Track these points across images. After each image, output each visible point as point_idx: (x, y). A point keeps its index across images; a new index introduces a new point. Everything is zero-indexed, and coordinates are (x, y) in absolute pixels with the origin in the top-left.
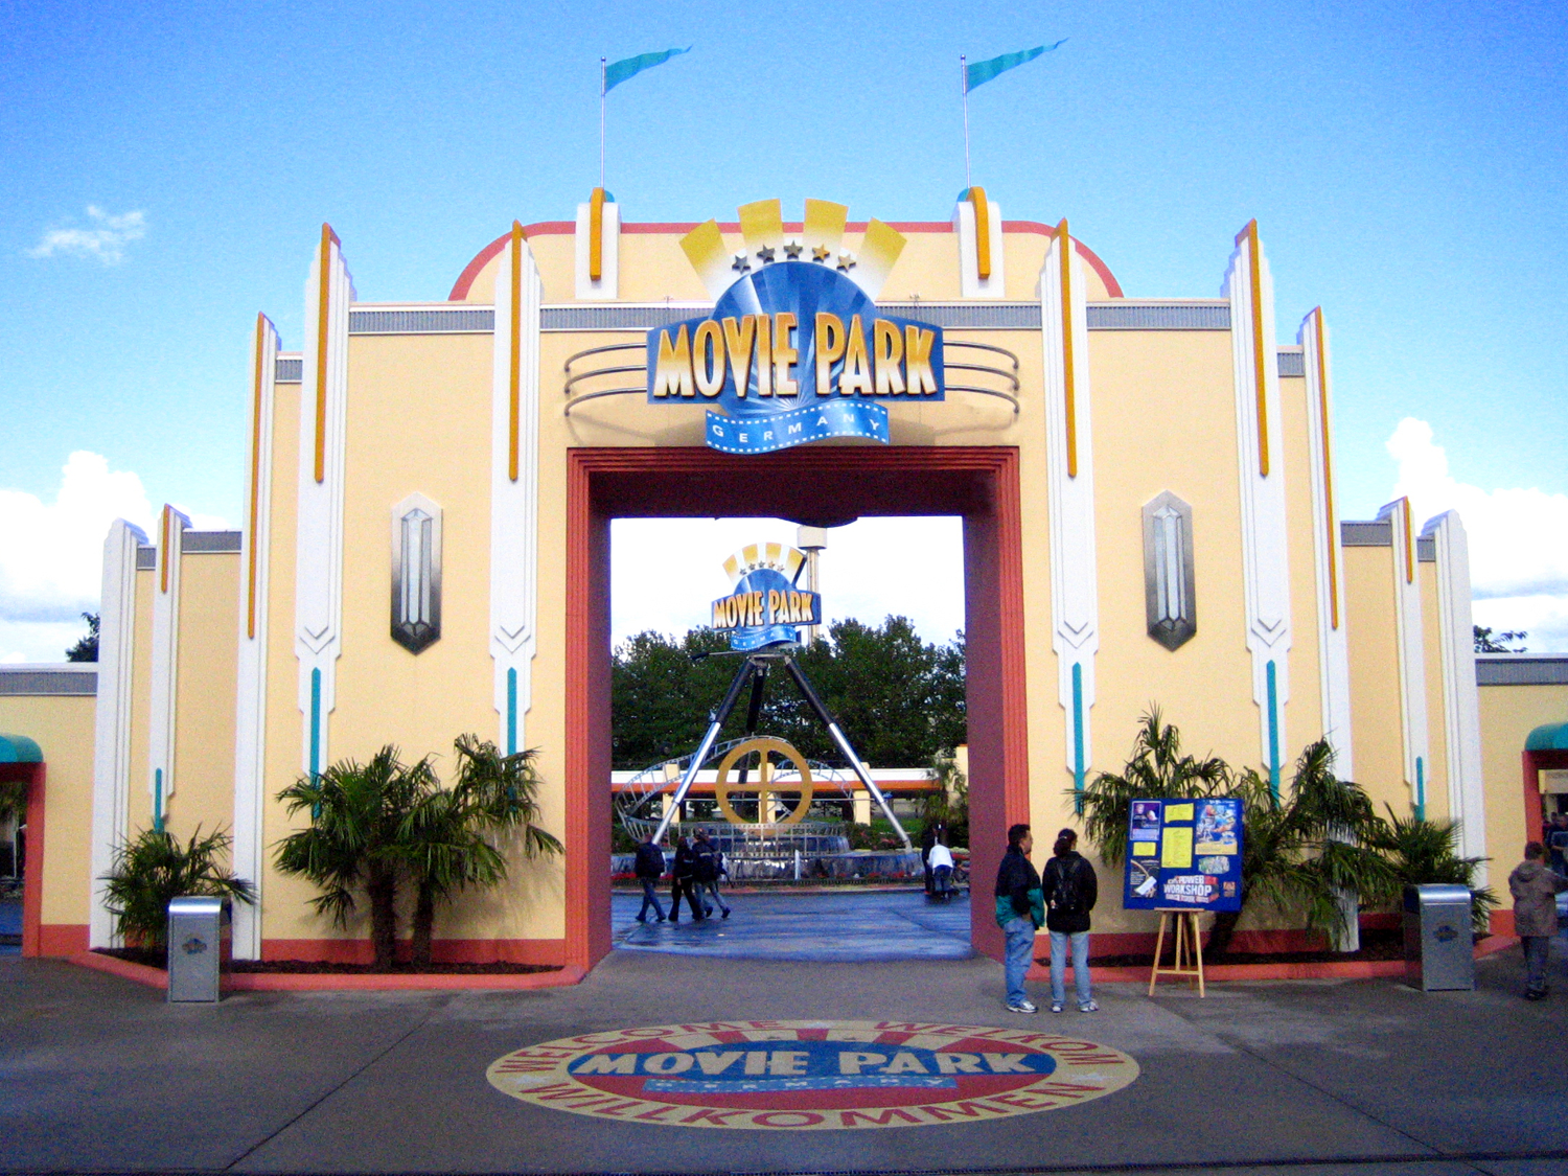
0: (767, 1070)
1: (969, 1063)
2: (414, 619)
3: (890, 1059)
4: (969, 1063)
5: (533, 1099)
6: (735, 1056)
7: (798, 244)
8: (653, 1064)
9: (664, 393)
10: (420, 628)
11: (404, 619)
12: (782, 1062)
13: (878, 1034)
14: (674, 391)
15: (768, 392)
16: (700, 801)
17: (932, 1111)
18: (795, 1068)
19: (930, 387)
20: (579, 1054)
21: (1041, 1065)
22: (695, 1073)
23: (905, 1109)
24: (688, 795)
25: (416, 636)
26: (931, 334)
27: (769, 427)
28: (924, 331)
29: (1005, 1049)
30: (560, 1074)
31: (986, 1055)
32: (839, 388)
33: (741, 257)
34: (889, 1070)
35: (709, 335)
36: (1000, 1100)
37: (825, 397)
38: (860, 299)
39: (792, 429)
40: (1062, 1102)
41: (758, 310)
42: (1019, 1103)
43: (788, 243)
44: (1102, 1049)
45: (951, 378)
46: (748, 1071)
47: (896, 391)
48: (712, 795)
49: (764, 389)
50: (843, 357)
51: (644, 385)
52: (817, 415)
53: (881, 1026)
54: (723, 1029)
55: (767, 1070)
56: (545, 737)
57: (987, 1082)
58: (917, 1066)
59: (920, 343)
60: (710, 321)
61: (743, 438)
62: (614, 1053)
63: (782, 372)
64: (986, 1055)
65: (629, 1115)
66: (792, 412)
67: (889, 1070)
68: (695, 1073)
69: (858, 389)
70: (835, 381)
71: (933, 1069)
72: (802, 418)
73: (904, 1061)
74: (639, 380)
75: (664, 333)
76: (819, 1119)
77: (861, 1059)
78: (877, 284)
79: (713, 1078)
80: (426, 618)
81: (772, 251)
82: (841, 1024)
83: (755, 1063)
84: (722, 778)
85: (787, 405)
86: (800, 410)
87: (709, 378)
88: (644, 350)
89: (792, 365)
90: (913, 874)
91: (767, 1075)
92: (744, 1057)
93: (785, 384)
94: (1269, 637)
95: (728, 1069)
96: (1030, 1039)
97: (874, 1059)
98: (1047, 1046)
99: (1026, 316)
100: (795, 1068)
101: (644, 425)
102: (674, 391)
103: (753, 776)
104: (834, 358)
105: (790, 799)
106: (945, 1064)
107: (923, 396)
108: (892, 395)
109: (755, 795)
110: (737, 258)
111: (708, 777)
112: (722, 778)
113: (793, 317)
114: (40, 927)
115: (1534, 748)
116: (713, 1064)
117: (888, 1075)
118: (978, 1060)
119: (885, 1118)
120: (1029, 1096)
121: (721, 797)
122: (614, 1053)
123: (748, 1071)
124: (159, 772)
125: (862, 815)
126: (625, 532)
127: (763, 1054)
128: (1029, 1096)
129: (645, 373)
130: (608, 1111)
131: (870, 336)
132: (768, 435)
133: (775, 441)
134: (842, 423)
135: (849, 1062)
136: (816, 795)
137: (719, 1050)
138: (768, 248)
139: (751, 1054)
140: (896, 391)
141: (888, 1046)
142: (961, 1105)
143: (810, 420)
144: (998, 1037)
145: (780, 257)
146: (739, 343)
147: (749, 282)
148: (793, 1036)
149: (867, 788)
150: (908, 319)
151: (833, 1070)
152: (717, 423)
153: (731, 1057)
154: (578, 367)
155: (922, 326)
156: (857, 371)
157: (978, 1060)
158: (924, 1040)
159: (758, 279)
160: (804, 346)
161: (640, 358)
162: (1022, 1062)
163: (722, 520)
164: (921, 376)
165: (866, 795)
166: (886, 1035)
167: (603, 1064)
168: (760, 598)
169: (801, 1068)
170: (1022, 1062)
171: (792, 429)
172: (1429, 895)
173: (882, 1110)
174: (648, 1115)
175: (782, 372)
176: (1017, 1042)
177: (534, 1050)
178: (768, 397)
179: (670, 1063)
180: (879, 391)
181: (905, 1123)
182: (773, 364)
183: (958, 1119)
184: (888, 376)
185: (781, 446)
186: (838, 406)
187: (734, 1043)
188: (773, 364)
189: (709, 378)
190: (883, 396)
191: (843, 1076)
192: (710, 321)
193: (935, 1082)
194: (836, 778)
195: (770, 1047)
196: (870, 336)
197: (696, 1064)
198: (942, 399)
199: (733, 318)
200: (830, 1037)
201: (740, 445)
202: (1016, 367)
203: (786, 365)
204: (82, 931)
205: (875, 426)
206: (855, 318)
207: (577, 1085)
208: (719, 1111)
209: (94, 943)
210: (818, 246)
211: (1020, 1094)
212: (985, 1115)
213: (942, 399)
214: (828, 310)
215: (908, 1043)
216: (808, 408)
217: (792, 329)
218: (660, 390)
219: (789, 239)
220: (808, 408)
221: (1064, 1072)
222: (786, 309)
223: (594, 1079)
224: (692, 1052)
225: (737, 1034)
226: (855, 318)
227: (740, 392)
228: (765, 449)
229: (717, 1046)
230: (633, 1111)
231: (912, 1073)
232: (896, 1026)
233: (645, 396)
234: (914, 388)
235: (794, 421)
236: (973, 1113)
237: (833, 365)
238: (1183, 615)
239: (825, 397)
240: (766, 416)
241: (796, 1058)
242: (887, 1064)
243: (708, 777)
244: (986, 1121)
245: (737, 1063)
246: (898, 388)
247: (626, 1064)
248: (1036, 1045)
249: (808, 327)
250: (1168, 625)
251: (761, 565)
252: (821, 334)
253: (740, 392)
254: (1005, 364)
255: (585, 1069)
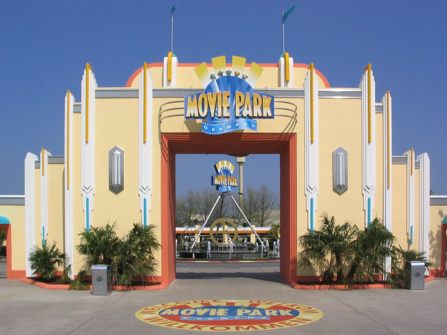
0: (216, 314)
1: (274, 313)
2: (116, 183)
3: (252, 311)
4: (274, 313)
5: (148, 322)
6: (208, 310)
7: (230, 70)
8: (183, 312)
9: (189, 116)
10: (118, 186)
11: (113, 183)
12: (221, 312)
13: (250, 304)
14: (192, 115)
15: (221, 116)
16: (205, 236)
17: (261, 326)
18: (224, 314)
19: (270, 115)
20: (162, 309)
21: (295, 313)
22: (195, 315)
23: (254, 326)
24: (201, 234)
25: (116, 189)
26: (271, 98)
27: (221, 126)
28: (268, 97)
29: (285, 309)
30: (156, 315)
31: (280, 311)
32: (242, 115)
33: (213, 74)
34: (251, 315)
35: (203, 98)
36: (282, 323)
37: (238, 118)
38: (249, 87)
39: (228, 127)
40: (300, 324)
41: (218, 91)
42: (287, 324)
43: (227, 70)
44: (313, 309)
45: (276, 112)
46: (211, 314)
47: (259, 116)
48: (208, 234)
49: (220, 115)
50: (244, 105)
51: (183, 113)
52: (236, 123)
53: (251, 302)
54: (205, 302)
55: (216, 314)
56: (154, 218)
57: (279, 318)
58: (259, 313)
59: (267, 101)
60: (203, 94)
61: (213, 130)
62: (173, 308)
63: (225, 110)
64: (280, 311)
65: (175, 326)
66: (228, 122)
67: (251, 315)
68: (195, 315)
69: (248, 115)
70: (241, 113)
71: (264, 314)
72: (231, 124)
73: (256, 312)
74: (182, 112)
75: (189, 98)
76: (229, 328)
77: (244, 311)
78: (255, 83)
79: (200, 316)
80: (120, 183)
81: (222, 72)
82: (238, 301)
83: (213, 312)
84: (211, 230)
85: (226, 120)
86: (230, 121)
87: (203, 112)
88: (184, 103)
89: (228, 108)
90: (44, 277)
91: (216, 316)
92: (210, 310)
93: (226, 114)
94: (145, 191)
95: (205, 314)
96: (293, 306)
97: (247, 311)
98: (297, 308)
99: (300, 93)
100: (224, 314)
101: (178, 126)
102: (192, 115)
103: (221, 229)
104: (241, 105)
105: (232, 235)
106: (268, 313)
107: (268, 117)
108: (259, 117)
109: (222, 234)
110: (212, 75)
111: (208, 229)
112: (211, 230)
113: (229, 93)
114: (12, 271)
115: (444, 223)
116: (201, 312)
117: (251, 316)
118: (277, 312)
119: (248, 328)
120: (290, 322)
121: (211, 235)
122: (173, 308)
123: (211, 314)
124: (43, 227)
125: (253, 240)
126: (179, 157)
127: (216, 310)
128: (290, 322)
129: (184, 110)
130: (169, 325)
131: (252, 99)
132: (221, 129)
133: (223, 131)
134: (244, 126)
135: (240, 312)
136: (239, 234)
137: (203, 308)
138: (221, 71)
139: (212, 310)
140: (259, 116)
141: (252, 307)
142: (270, 325)
143: (234, 124)
144: (284, 305)
145: (225, 74)
146: (212, 101)
147: (215, 81)
148: (225, 305)
149: (254, 233)
150: (263, 93)
151: (235, 314)
152: (205, 125)
153: (206, 310)
154: (164, 108)
155: (268, 96)
156: (248, 110)
157: (277, 312)
158: (263, 306)
159: (218, 81)
160: (232, 102)
161: (182, 105)
162: (290, 313)
163: (209, 155)
164: (267, 111)
165: (254, 235)
166: (252, 304)
167: (169, 312)
168: (228, 97)
169: (226, 314)
170: (290, 313)
171: (228, 127)
172: (413, 264)
173: (247, 326)
174: (180, 327)
175: (225, 110)
176: (289, 307)
177: (150, 308)
178: (220, 117)
179: (189, 312)
180: (254, 116)
181: (254, 330)
182: (222, 108)
183: (269, 329)
184: (257, 111)
185: (225, 132)
186: (242, 120)
187: (207, 306)
188: (222, 108)
189: (203, 112)
190: (255, 117)
191: (238, 316)
192: (203, 94)
193: (264, 318)
194: (245, 230)
195: (217, 308)
196: (252, 99)
197: (196, 312)
198: (274, 118)
199: (210, 93)
200: (235, 305)
201: (212, 132)
202: (296, 109)
203: (226, 108)
204: (24, 272)
205: (253, 126)
206: (248, 93)
207: (161, 318)
208: (201, 326)
209: (27, 276)
210: (236, 71)
211: (288, 321)
212: (277, 328)
213: (274, 118)
214: (239, 91)
215: (258, 307)
216: (233, 121)
217: (228, 97)
218: (188, 115)
219: (227, 69)
220: (233, 121)
221: (302, 315)
222: (227, 90)
223: (166, 316)
224: (195, 309)
225: (209, 304)
226: (248, 93)
227: (213, 116)
228: (220, 133)
229: (203, 307)
230: (176, 325)
231: (258, 315)
232: (255, 302)
233: (184, 117)
234: (265, 115)
235: (229, 125)
236: (274, 327)
237: (241, 108)
238: (344, 184)
239: (238, 118)
240: (220, 123)
241: (225, 311)
242: (251, 313)
243: (208, 229)
244: (277, 329)
245: (208, 312)
246: (260, 115)
247: (176, 312)
248: (294, 308)
249: (234, 95)
250: (115, 186)
251: (226, 167)
252: (237, 98)
253: (213, 116)
254: (293, 108)
255: (164, 313)
